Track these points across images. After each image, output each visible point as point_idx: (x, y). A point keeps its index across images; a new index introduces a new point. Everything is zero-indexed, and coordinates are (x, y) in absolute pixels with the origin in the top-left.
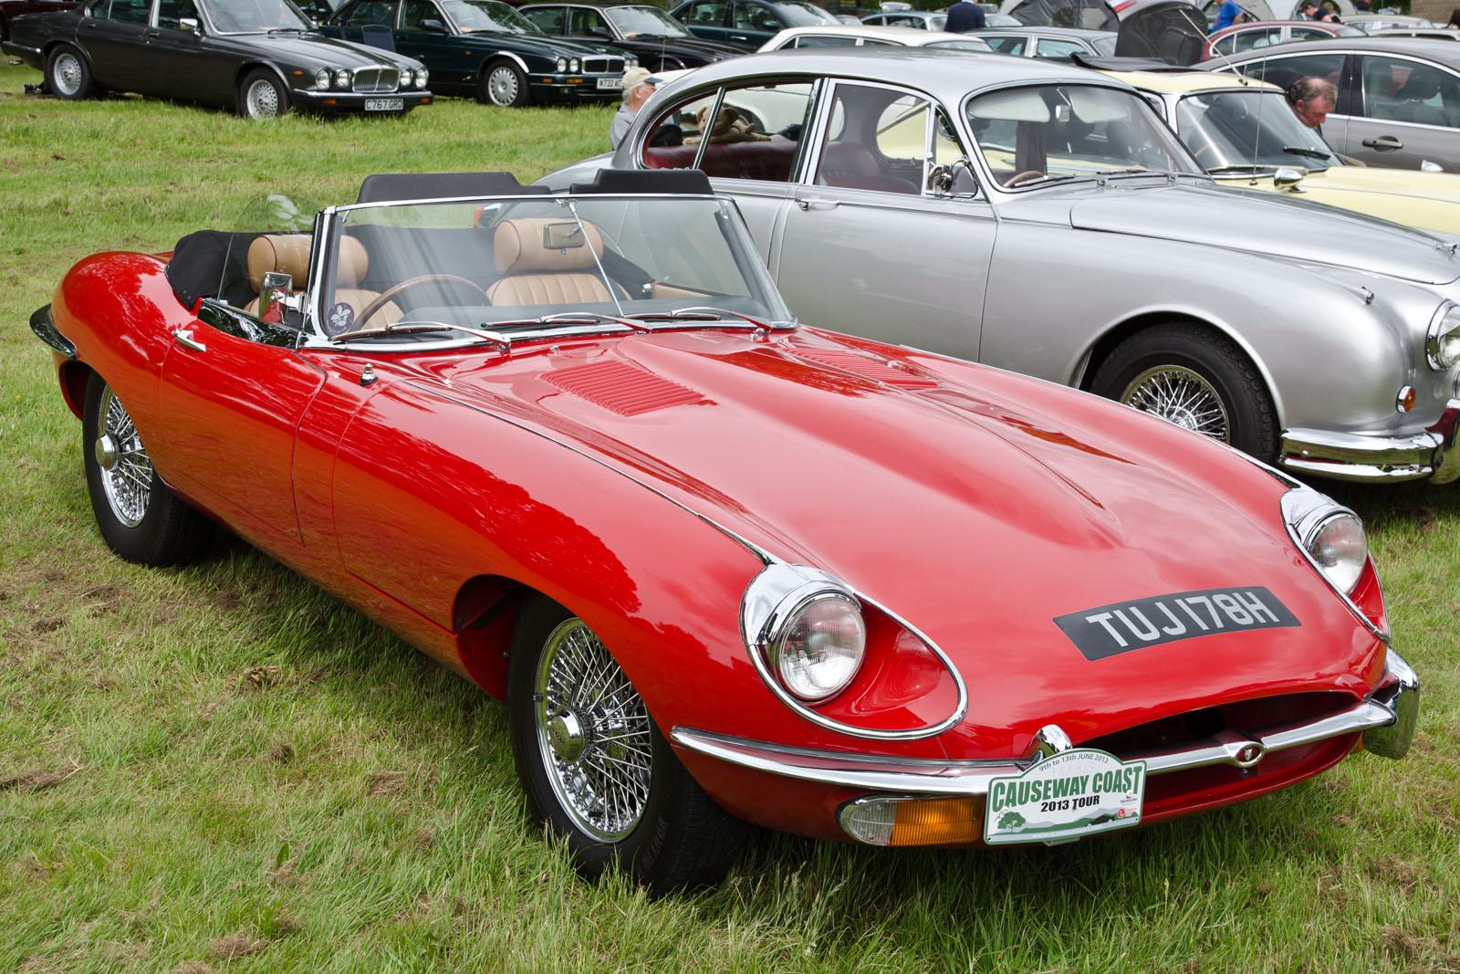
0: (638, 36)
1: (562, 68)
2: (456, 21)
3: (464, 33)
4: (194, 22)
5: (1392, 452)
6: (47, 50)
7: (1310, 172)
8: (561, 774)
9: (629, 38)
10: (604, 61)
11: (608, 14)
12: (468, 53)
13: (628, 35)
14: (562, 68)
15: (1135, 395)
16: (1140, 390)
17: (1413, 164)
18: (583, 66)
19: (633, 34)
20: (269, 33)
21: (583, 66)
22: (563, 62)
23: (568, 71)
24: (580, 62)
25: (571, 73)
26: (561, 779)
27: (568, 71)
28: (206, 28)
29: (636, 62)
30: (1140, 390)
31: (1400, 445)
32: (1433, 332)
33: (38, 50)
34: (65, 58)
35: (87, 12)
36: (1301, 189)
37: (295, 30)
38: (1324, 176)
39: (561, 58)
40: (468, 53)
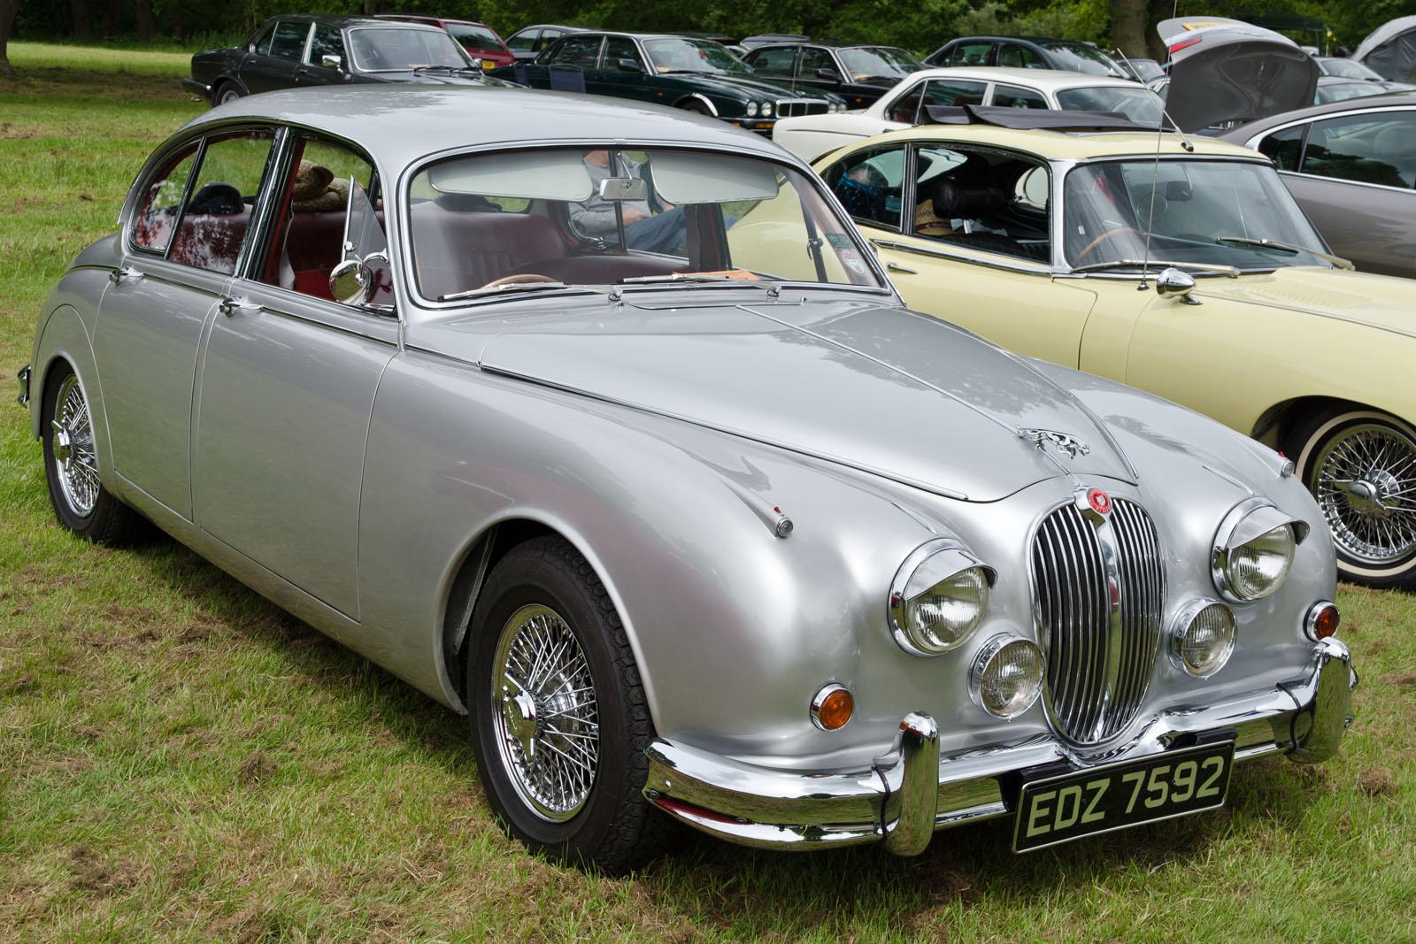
0: (869, 79)
1: (752, 112)
2: (849, 69)
3: (660, 73)
4: (337, 59)
5: (821, 800)
6: (215, 88)
7: (1242, 274)
8: (521, 771)
9: (858, 81)
10: (804, 105)
11: (837, 54)
12: (661, 94)
13: (857, 77)
14: (752, 112)
15: (1329, 462)
16: (1333, 456)
17: (1342, 268)
18: (777, 109)
19: (863, 76)
20: (415, 70)
21: (777, 109)
22: (754, 105)
23: (759, 115)
24: (774, 106)
25: (763, 117)
26: (521, 774)
27: (759, 115)
28: (350, 66)
29: (843, 106)
30: (1333, 456)
31: (836, 787)
32: (1221, 543)
33: (209, 87)
34: (230, 95)
35: (252, 48)
36: (1196, 298)
37: (447, 68)
38: (1273, 280)
39: (751, 101)
40: (661, 94)
